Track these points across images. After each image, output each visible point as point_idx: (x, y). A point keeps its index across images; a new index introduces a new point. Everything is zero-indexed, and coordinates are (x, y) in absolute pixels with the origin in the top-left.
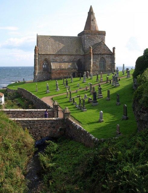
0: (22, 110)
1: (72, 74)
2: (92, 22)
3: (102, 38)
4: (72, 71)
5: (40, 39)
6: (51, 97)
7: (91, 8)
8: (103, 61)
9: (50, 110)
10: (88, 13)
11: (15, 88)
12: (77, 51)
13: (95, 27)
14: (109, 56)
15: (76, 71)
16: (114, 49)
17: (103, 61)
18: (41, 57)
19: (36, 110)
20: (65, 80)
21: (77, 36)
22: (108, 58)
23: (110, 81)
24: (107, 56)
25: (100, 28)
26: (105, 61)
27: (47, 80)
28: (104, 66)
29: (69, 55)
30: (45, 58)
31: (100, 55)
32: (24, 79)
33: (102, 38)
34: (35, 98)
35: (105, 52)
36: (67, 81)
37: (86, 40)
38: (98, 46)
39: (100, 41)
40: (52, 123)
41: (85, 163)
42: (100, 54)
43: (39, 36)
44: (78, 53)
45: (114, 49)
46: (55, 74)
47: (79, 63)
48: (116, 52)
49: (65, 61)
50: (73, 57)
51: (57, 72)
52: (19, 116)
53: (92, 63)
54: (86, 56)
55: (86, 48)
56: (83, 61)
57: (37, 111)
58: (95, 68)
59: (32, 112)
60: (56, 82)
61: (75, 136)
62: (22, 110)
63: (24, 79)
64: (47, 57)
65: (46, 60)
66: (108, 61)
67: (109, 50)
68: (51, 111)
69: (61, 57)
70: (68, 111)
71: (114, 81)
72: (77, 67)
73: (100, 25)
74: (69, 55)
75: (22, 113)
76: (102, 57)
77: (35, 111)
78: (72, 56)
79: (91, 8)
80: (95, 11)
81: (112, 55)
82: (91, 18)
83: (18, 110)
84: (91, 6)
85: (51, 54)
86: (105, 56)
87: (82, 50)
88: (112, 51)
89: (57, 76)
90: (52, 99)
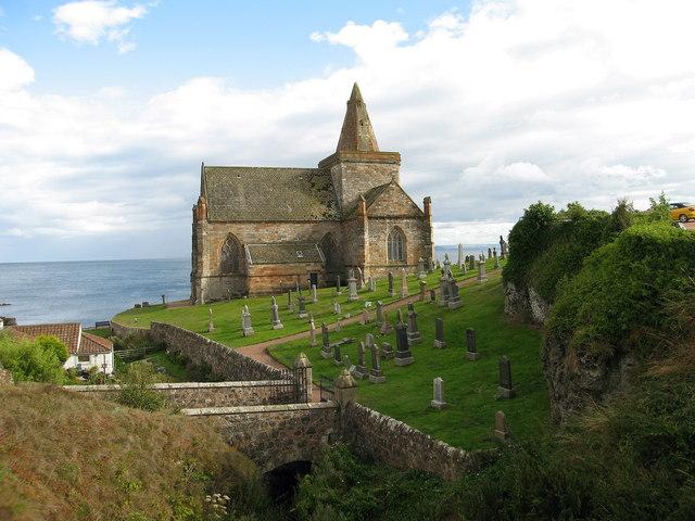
1: (308, 276)
2: (359, 127)
10: (349, 103)
11: (143, 324)
13: (371, 142)
15: (318, 267)
16: (427, 201)
25: (383, 145)
27: (235, 297)
34: (219, 353)
40: (305, 419)
42: (390, 218)
45: (427, 201)
47: (328, 245)
48: (432, 212)
51: (265, 272)
52: (197, 404)
53: (367, 245)
54: (350, 220)
55: (345, 202)
56: (338, 238)
58: (377, 258)
60: (273, 301)
61: (382, 453)
66: (411, 235)
67: (415, 206)
69: (274, 228)
73: (383, 130)
75: (207, 395)
77: (243, 387)
80: (366, 96)
82: (356, 116)
84: (355, 86)
86: (402, 224)
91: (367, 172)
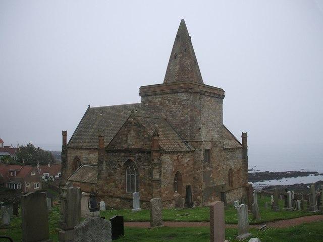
7: (183, 26)
16: (244, 136)
21: (138, 100)
45: (244, 136)
79: (183, 26)
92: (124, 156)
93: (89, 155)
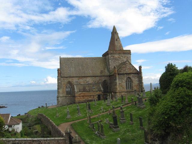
0: (30, 139)
1: (97, 96)
2: (116, 42)
3: (128, 57)
4: (97, 93)
5: (169, 65)
6: (72, 123)
8: (129, 81)
9: (62, 138)
12: (102, 72)
14: (136, 75)
15: (101, 93)
16: (140, 67)
17: (129, 81)
18: (63, 80)
19: (45, 139)
20: (88, 103)
22: (135, 77)
23: (135, 102)
24: (133, 76)
26: (131, 81)
28: (131, 87)
29: (93, 76)
30: (68, 81)
31: (125, 75)
32: (46, 104)
33: (128, 57)
35: (131, 71)
36: (89, 105)
37: (110, 61)
38: (123, 66)
39: (125, 60)
41: (188, 119)
42: (126, 74)
43: (62, 58)
44: (103, 74)
45: (140, 67)
46: (79, 98)
47: (105, 84)
48: (142, 71)
49: (90, 83)
50: (98, 79)
56: (109, 81)
57: (46, 140)
59: (40, 142)
62: (30, 139)
63: (46, 104)
64: (70, 80)
65: (69, 83)
66: (135, 81)
67: (136, 69)
68: (62, 140)
69: (85, 79)
70: (78, 140)
71: (139, 102)
72: (102, 89)
74: (93, 76)
76: (129, 78)
77: (44, 140)
78: (97, 78)
81: (139, 74)
83: (25, 139)
85: (74, 76)
86: (131, 76)
87: (106, 71)
88: (138, 69)
89: (81, 99)
90: (71, 125)
91: (119, 57)
92: (126, 76)
93: (79, 80)
